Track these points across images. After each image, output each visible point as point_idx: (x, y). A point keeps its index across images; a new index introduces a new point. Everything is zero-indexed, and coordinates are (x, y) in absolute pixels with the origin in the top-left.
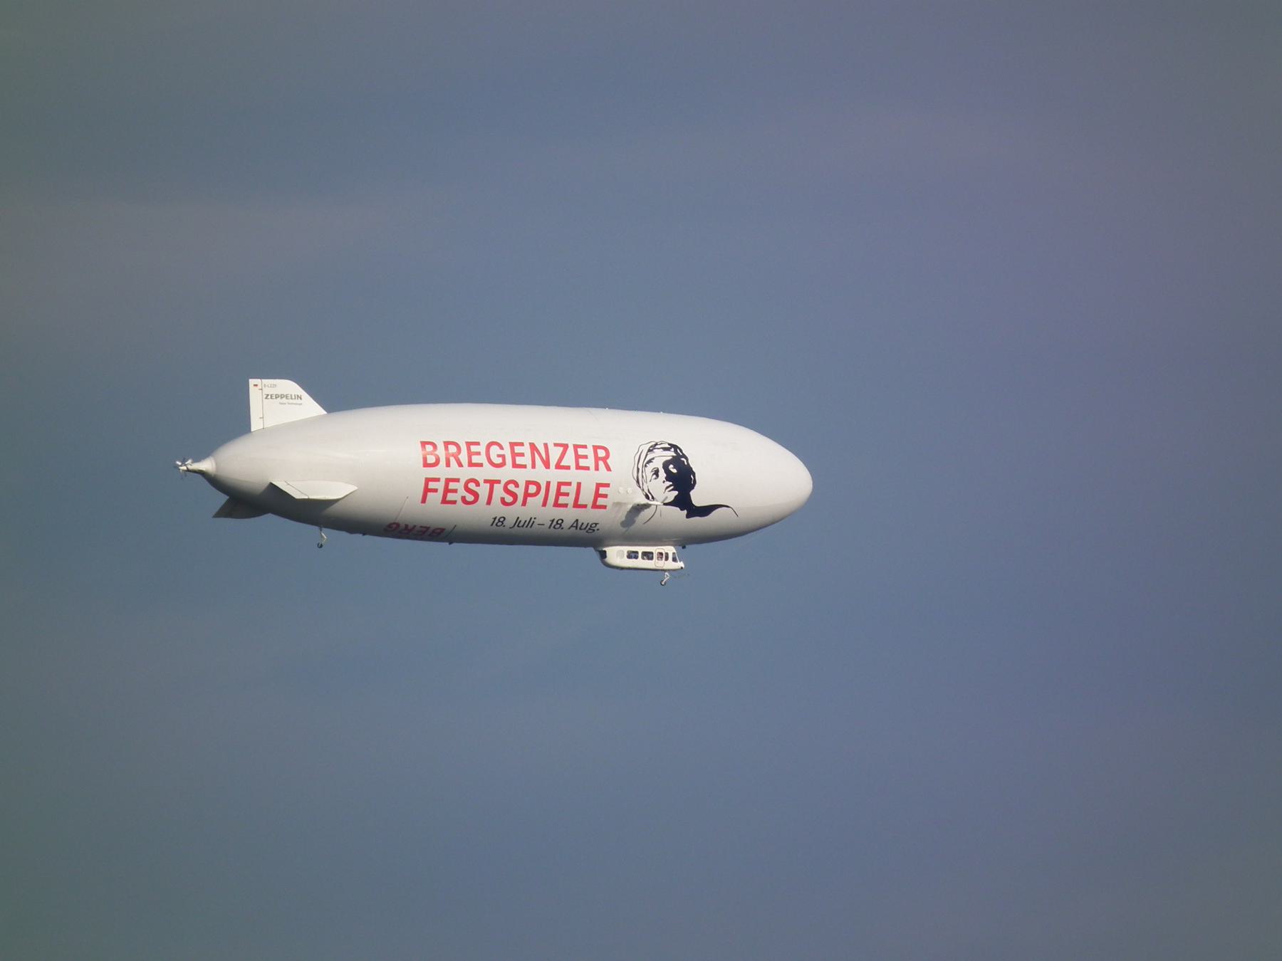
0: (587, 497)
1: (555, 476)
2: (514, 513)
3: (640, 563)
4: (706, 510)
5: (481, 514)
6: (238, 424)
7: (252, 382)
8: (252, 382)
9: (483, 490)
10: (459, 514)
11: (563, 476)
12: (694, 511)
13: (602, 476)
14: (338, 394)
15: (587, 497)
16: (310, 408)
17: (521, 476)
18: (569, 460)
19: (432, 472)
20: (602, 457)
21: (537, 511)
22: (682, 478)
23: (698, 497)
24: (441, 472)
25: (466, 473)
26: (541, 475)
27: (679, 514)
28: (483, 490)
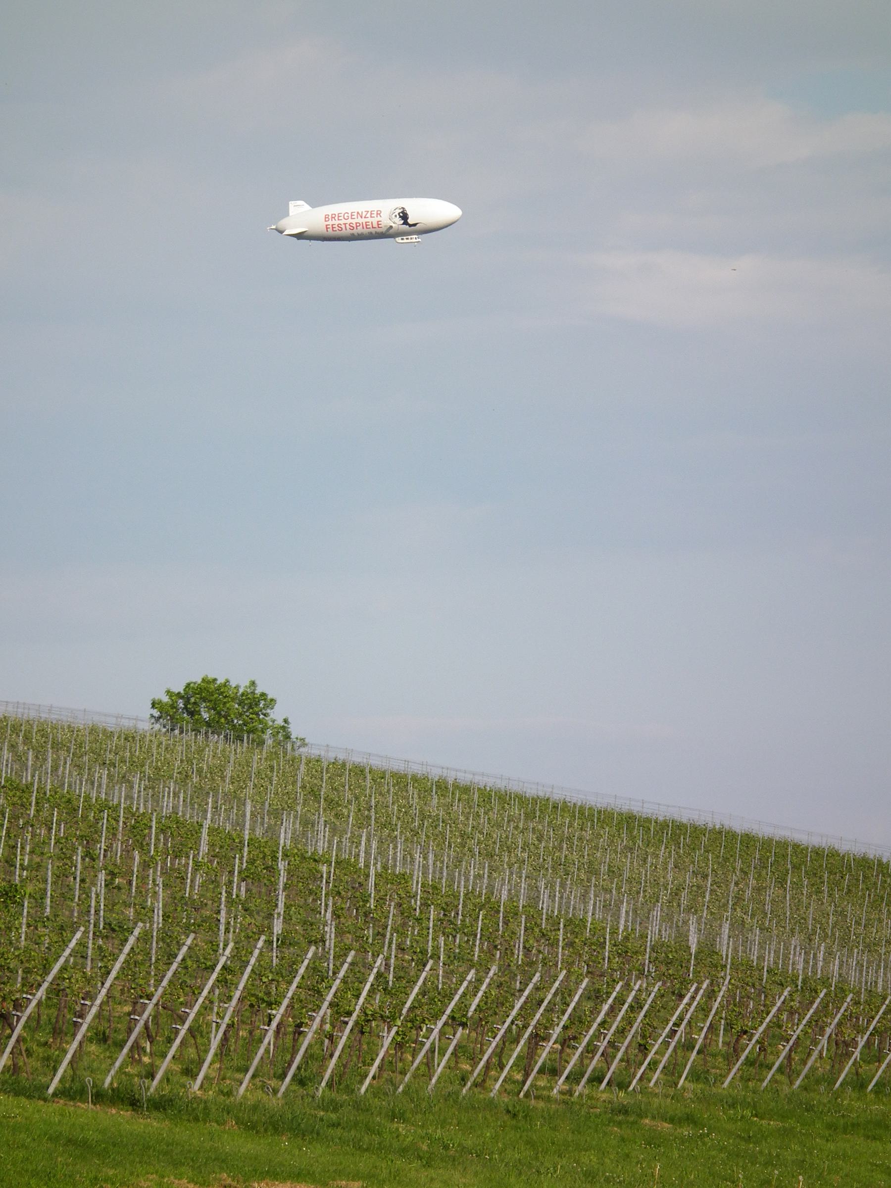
0: (375, 225)
1: (364, 220)
2: (355, 231)
3: (405, 241)
4: (415, 225)
5: (347, 232)
6: (286, 214)
7: (292, 204)
8: (292, 204)
9: (343, 226)
10: (338, 233)
11: (367, 220)
12: (410, 226)
13: (379, 219)
14: (314, 204)
15: (375, 225)
16: (307, 207)
17: (354, 221)
18: (368, 215)
19: (327, 223)
20: (379, 213)
21: (360, 230)
22: (404, 216)
23: (410, 221)
24: (330, 223)
25: (337, 222)
26: (360, 220)
27: (406, 227)
28: (343, 226)
